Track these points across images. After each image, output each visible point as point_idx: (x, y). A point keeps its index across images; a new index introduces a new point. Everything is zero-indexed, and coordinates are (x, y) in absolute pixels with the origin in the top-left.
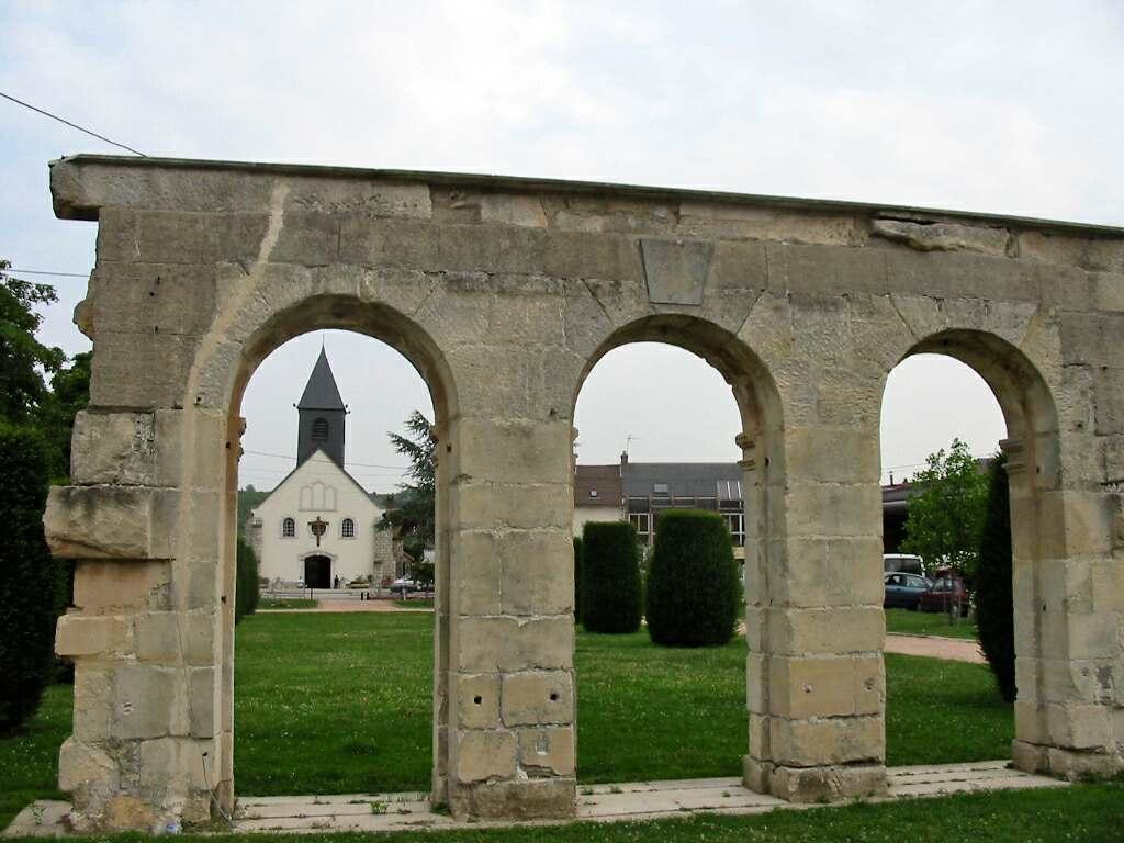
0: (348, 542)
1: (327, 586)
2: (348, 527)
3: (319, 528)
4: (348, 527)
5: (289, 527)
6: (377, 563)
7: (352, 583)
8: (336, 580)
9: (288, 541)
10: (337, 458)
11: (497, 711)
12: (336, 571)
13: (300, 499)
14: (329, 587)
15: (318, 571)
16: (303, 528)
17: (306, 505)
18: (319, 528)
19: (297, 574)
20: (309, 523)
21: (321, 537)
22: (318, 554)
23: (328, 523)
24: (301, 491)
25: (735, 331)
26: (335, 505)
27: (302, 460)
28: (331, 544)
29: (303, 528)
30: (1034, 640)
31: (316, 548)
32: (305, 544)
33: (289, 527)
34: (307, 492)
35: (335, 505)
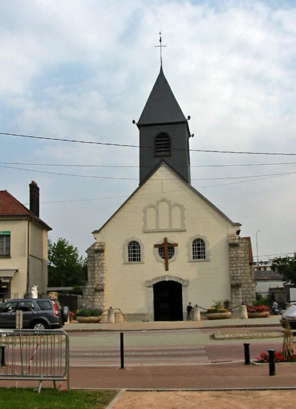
0: (200, 264)
1: (179, 317)
2: (199, 248)
3: (166, 250)
4: (199, 248)
5: (134, 251)
6: (235, 287)
7: (209, 311)
8: (189, 308)
9: (135, 266)
10: (182, 173)
11: (248, 391)
12: (188, 298)
13: (145, 220)
14: (180, 318)
15: (168, 300)
16: (149, 252)
17: (151, 226)
18: (166, 250)
19: (144, 302)
20: (156, 246)
21: (169, 260)
22: (167, 280)
23: (176, 245)
24: (145, 211)
25: (66, 388)
26: (183, 224)
27: (144, 178)
28: (181, 268)
29: (149, 252)
30: (96, 332)
31: (164, 273)
32: (153, 268)
33: (134, 251)
34: (151, 212)
35: (183, 224)
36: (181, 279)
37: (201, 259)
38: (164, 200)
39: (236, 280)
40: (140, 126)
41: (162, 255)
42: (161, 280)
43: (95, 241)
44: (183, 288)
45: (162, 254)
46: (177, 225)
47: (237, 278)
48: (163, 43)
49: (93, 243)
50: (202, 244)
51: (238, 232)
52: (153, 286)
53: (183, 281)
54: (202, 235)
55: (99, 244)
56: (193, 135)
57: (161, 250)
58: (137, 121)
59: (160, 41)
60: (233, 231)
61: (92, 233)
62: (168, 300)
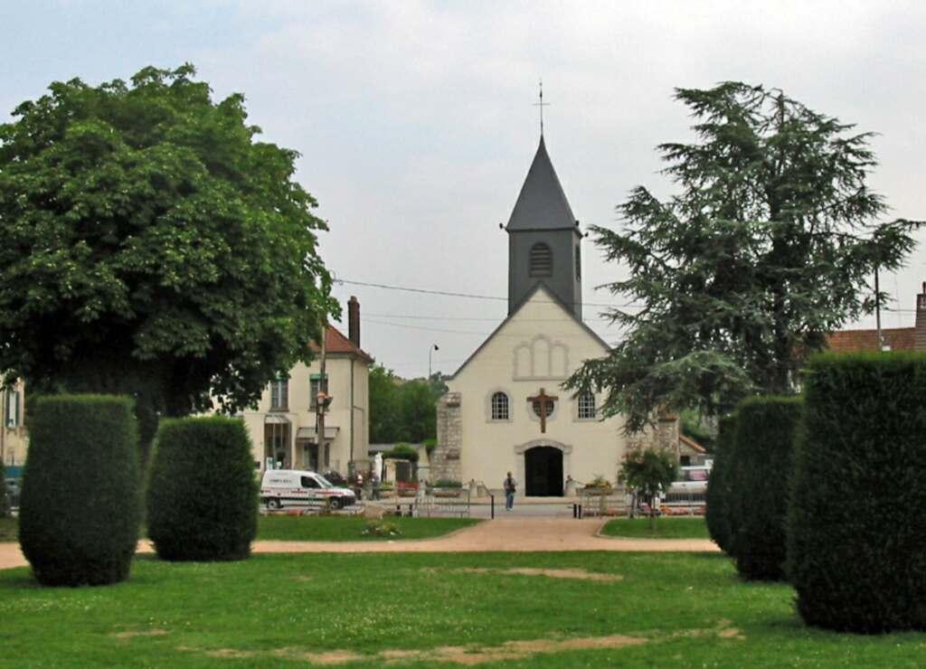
37: (502, 420)
42: (535, 445)
53: (564, 446)
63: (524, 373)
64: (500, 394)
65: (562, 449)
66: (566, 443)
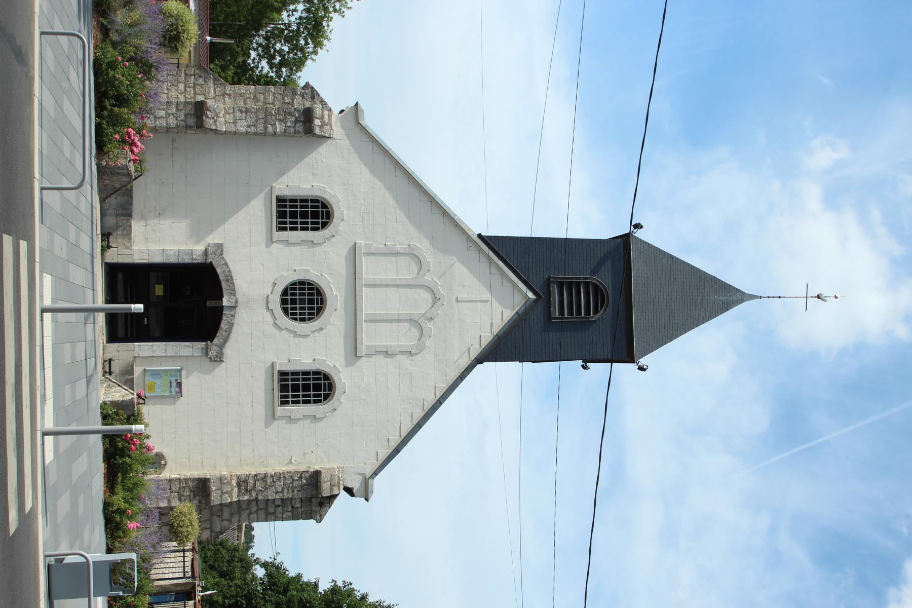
2: (306, 387)
4: (306, 387)
5: (304, 214)
15: (175, 304)
16: (309, 257)
28: (258, 339)
32: (257, 264)
34: (406, 270)
36: (225, 341)
37: (277, 394)
38: (436, 300)
39: (221, 489)
40: (623, 244)
41: (292, 289)
42: (224, 285)
43: (336, 111)
44: (201, 345)
45: (295, 289)
46: (369, 337)
47: (227, 492)
48: (813, 302)
49: (331, 104)
50: (320, 395)
51: (349, 491)
52: (208, 262)
53: (222, 346)
54: (342, 399)
55: (326, 121)
56: (585, 367)
57: (112, 200)
58: (639, 234)
59: (818, 297)
60: (356, 485)
61: (357, 104)
62: (175, 304)
63: (368, 268)
64: (331, 387)
65: (216, 341)
66: (228, 351)
